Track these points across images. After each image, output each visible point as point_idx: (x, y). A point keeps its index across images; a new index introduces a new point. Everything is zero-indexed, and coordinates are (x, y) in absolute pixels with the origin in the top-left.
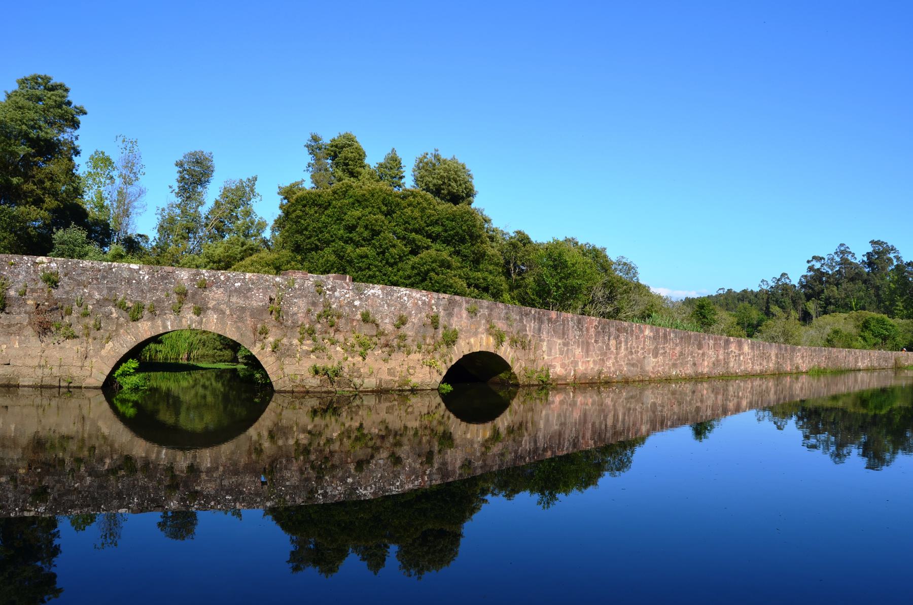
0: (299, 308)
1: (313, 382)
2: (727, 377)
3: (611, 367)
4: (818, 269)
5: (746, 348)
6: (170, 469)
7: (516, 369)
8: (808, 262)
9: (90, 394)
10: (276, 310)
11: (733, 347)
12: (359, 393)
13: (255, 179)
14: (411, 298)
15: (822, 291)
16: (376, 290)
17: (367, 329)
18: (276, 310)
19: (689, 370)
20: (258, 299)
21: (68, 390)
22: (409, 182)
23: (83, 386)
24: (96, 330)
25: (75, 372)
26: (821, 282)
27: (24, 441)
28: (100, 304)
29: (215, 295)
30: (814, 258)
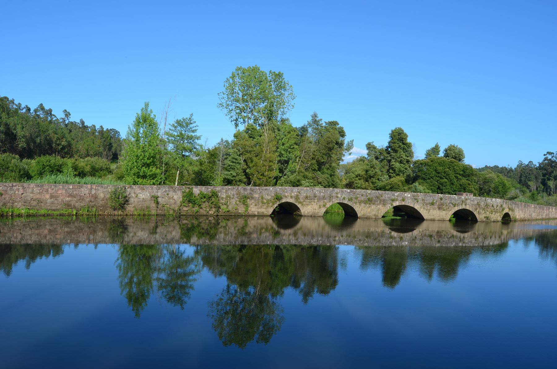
0: (482, 204)
1: (485, 219)
2: (549, 219)
3: (527, 216)
4: (550, 159)
5: (554, 210)
6: (460, 237)
7: (511, 217)
8: (544, 155)
9: (320, 218)
10: (478, 204)
11: (550, 210)
12: (491, 222)
13: (353, 141)
14: (499, 200)
15: (552, 172)
16: (494, 200)
17: (492, 208)
18: (478, 204)
19: (540, 217)
20: (476, 202)
21: (444, 221)
22: (441, 154)
23: (42, 212)
24: (448, 209)
25: (445, 217)
26: (552, 167)
27: (436, 231)
28: (449, 203)
29: (468, 201)
30: (548, 153)
